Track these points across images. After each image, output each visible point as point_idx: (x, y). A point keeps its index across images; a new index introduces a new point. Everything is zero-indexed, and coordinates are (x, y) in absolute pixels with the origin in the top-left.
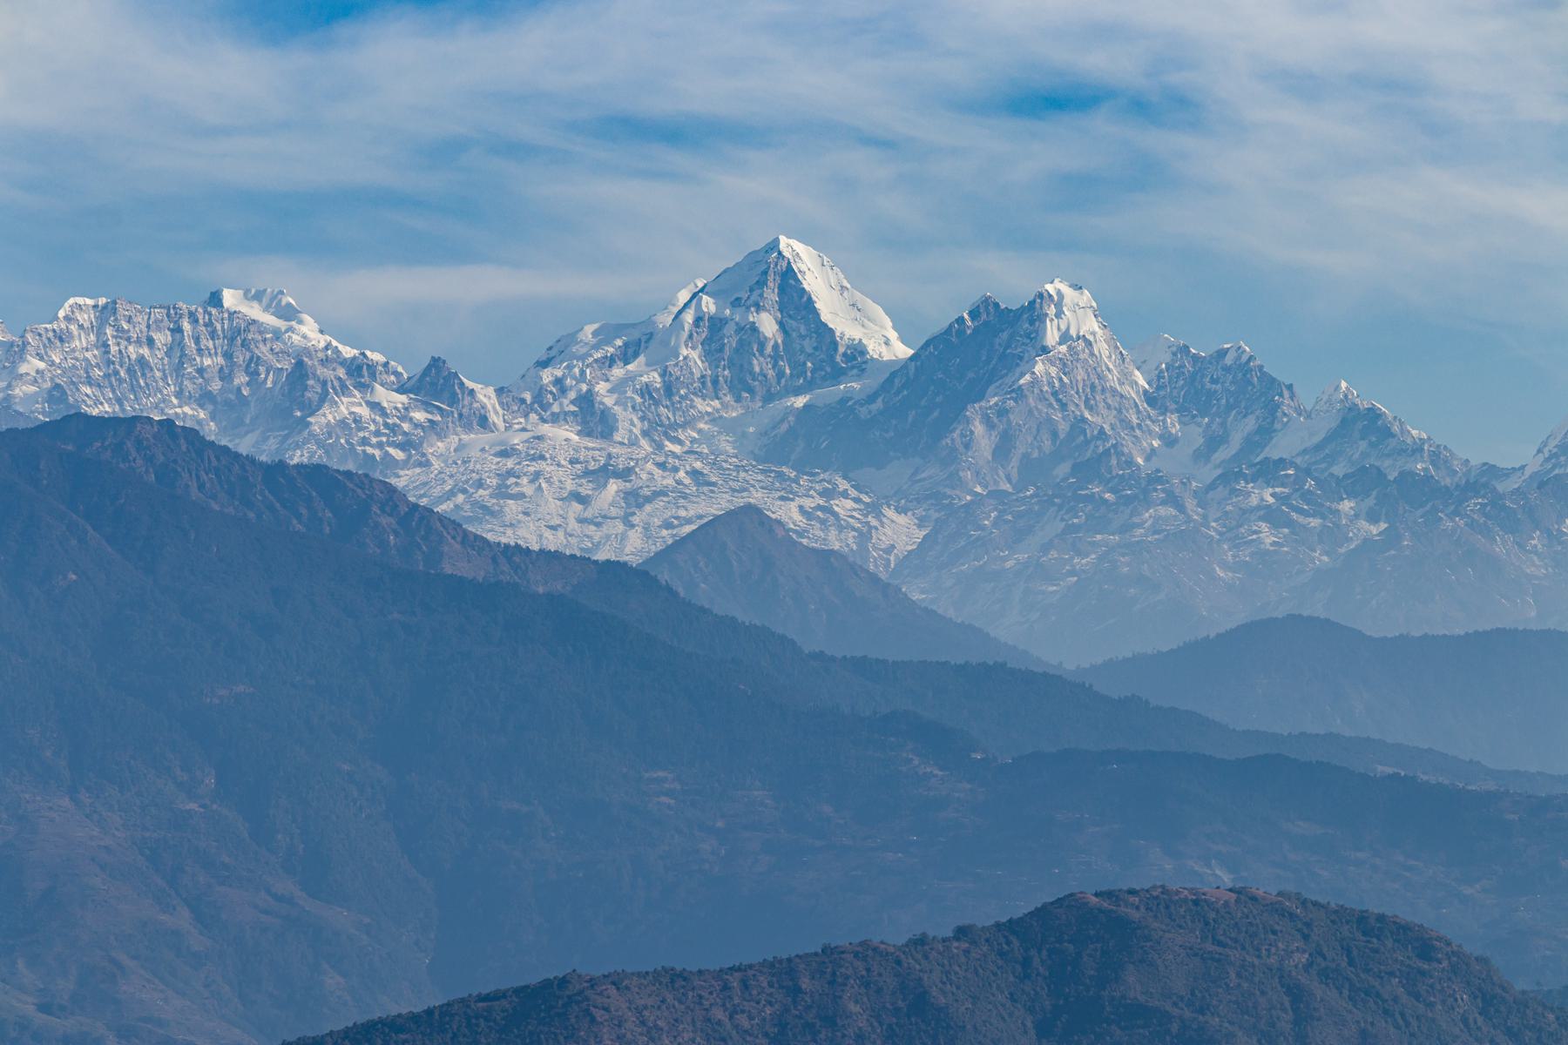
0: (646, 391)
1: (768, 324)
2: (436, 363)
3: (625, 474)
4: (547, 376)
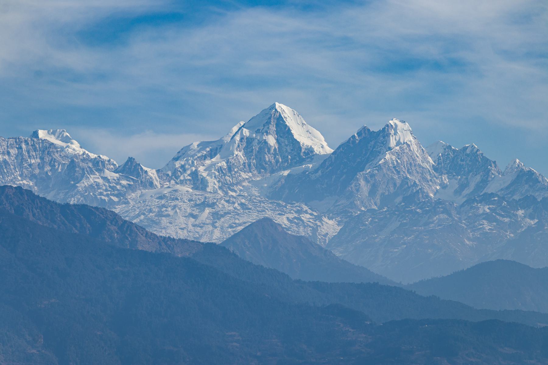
0: (220, 170)
1: (271, 140)
2: (131, 160)
3: (212, 205)
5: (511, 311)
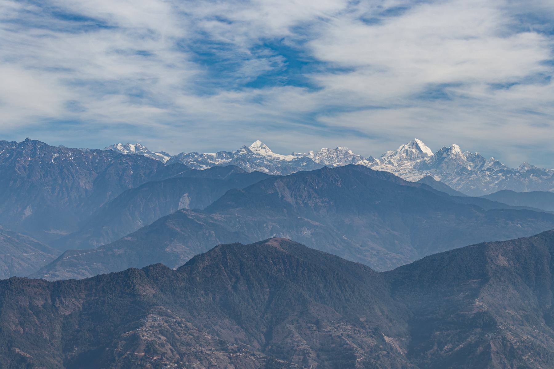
0: (398, 160)
1: (414, 151)
2: (371, 156)
3: (399, 171)
4: (383, 158)
5: (352, 263)
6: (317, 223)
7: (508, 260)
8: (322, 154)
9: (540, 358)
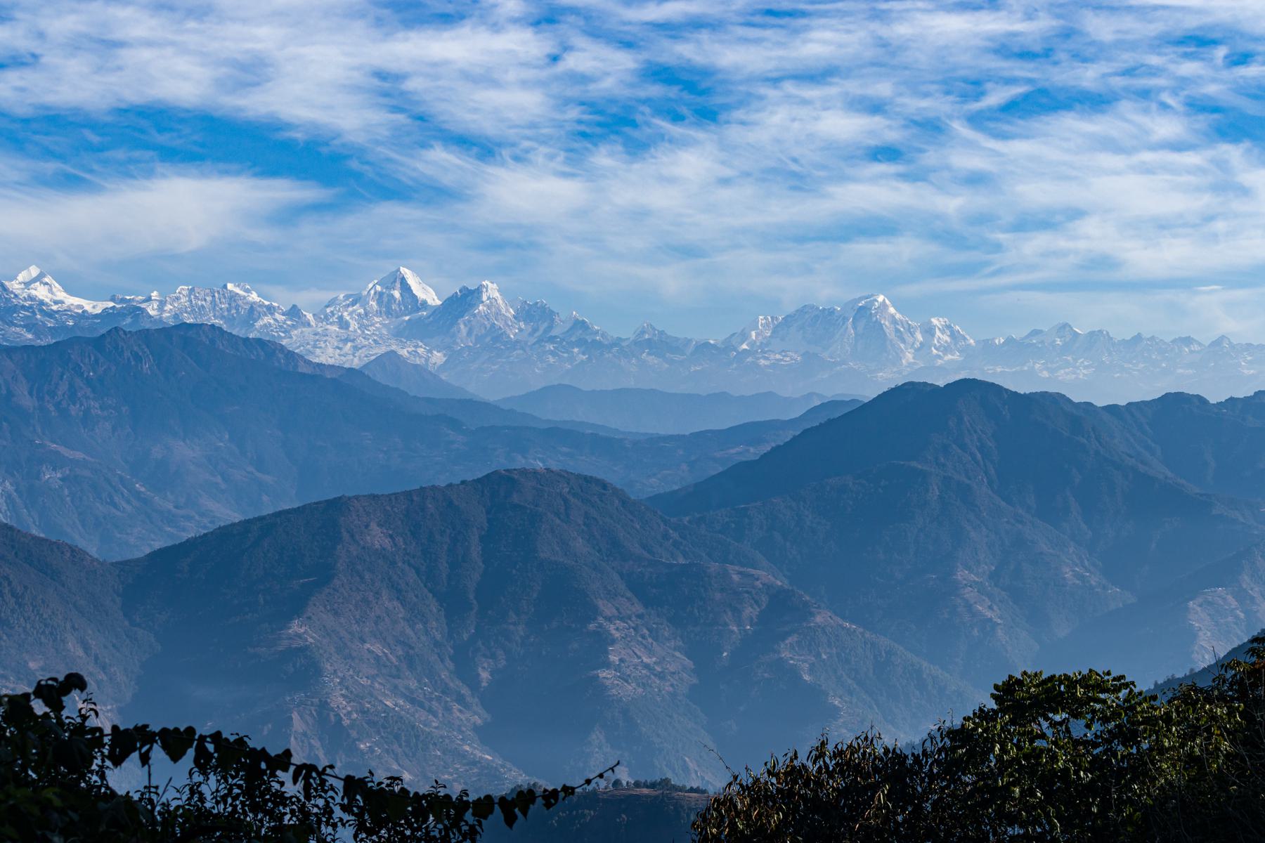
0: (359, 315)
3: (353, 341)
6: (79, 455)
7: (391, 536)
8: (178, 298)
9: (400, 746)
